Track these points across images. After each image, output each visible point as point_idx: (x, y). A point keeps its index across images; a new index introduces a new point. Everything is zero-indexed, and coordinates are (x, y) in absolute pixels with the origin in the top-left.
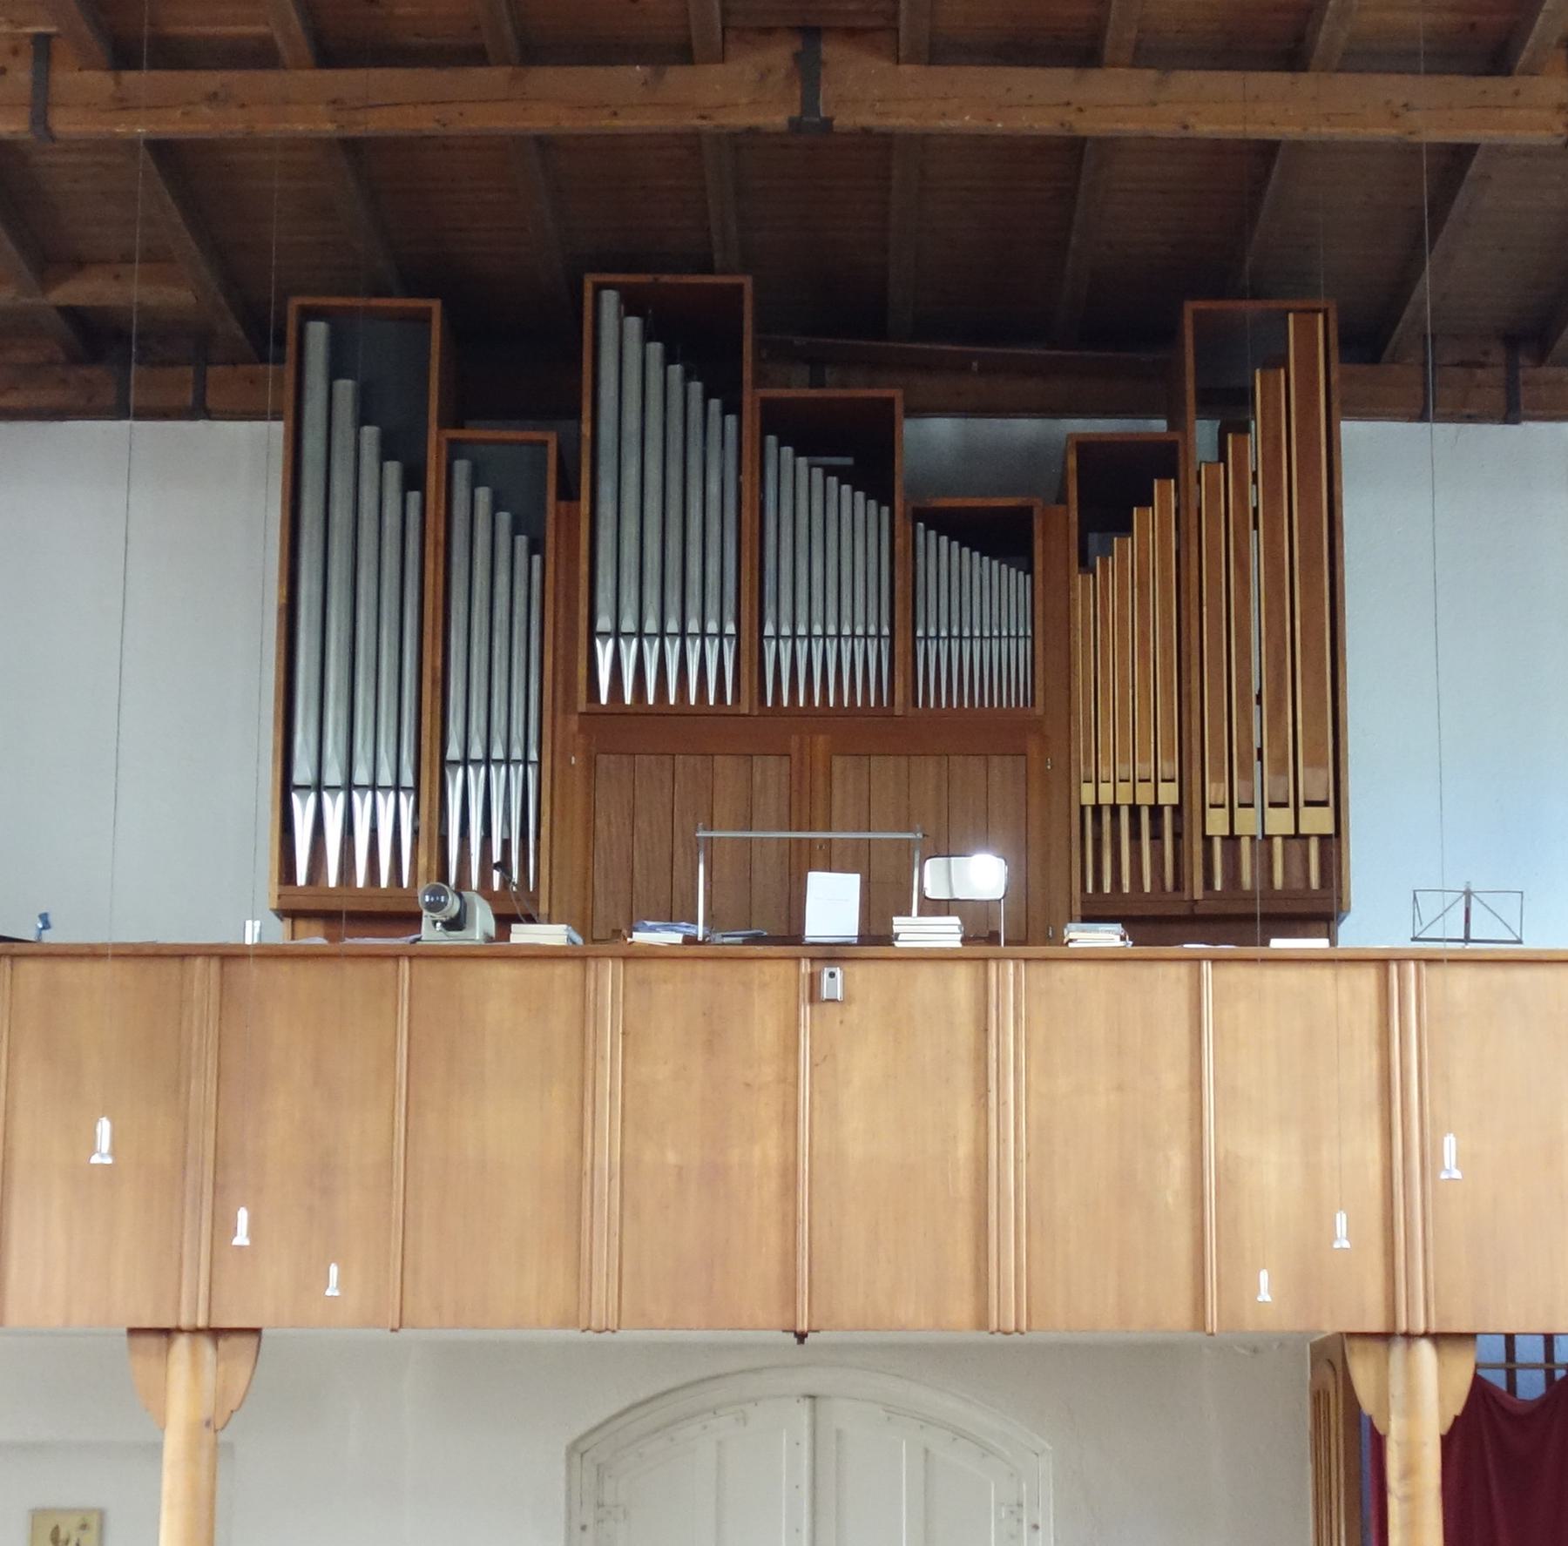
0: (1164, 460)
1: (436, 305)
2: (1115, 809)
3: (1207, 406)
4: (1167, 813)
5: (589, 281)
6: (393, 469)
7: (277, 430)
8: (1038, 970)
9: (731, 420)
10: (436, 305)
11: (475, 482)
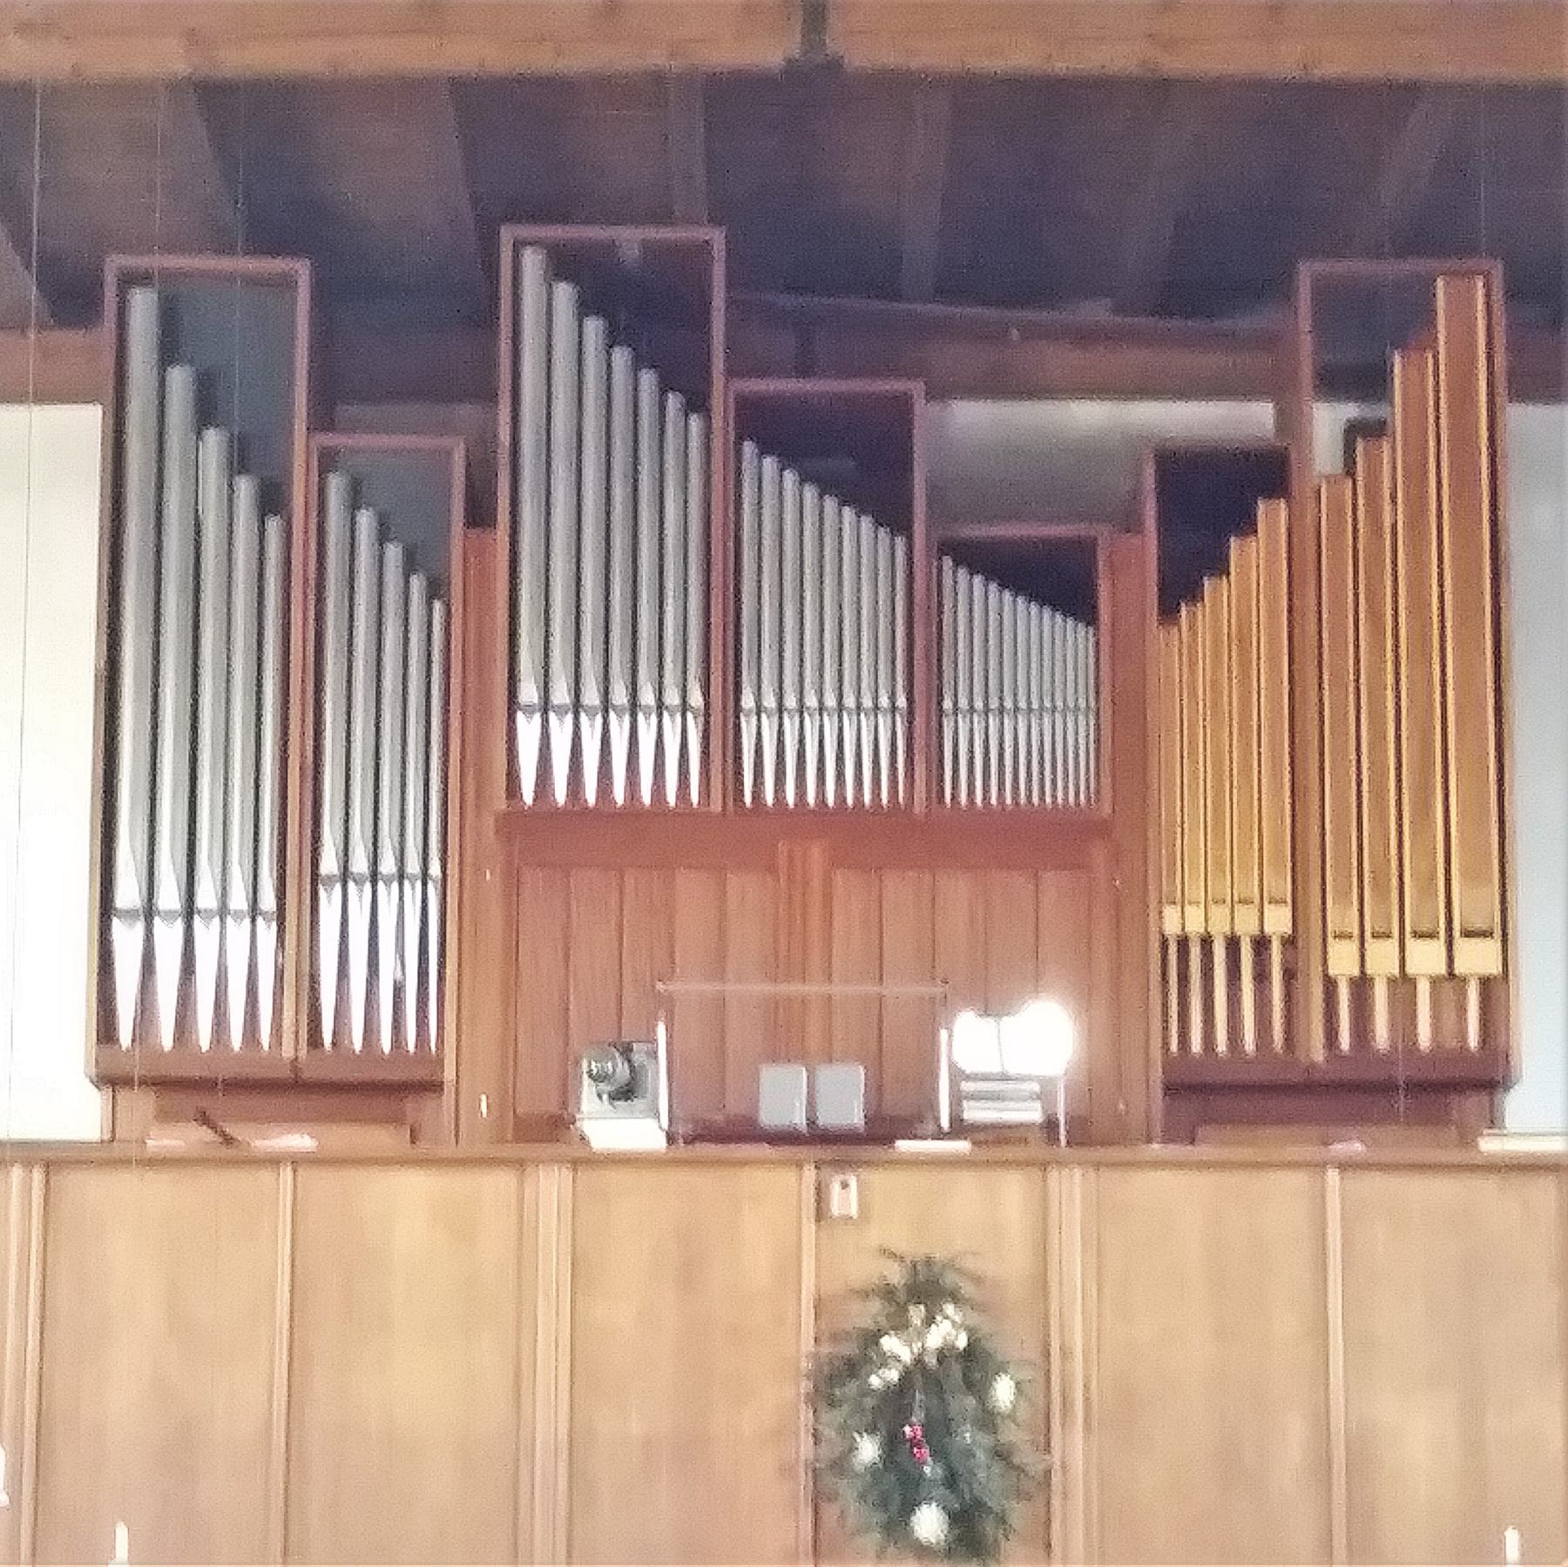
0: (1266, 471)
1: (302, 270)
2: (1207, 942)
3: (1332, 384)
4: (1276, 947)
5: (507, 234)
6: (245, 488)
7: (89, 419)
8: (1110, 1177)
9: (695, 423)
10: (302, 270)
11: (355, 502)
